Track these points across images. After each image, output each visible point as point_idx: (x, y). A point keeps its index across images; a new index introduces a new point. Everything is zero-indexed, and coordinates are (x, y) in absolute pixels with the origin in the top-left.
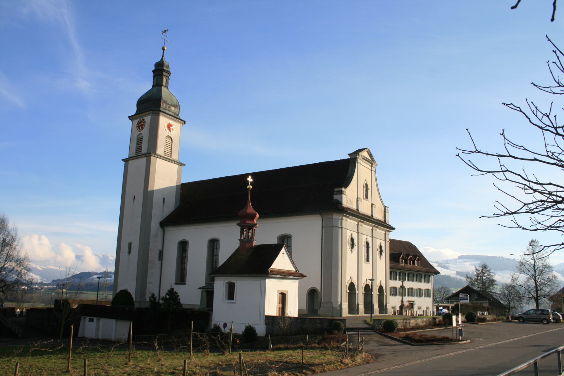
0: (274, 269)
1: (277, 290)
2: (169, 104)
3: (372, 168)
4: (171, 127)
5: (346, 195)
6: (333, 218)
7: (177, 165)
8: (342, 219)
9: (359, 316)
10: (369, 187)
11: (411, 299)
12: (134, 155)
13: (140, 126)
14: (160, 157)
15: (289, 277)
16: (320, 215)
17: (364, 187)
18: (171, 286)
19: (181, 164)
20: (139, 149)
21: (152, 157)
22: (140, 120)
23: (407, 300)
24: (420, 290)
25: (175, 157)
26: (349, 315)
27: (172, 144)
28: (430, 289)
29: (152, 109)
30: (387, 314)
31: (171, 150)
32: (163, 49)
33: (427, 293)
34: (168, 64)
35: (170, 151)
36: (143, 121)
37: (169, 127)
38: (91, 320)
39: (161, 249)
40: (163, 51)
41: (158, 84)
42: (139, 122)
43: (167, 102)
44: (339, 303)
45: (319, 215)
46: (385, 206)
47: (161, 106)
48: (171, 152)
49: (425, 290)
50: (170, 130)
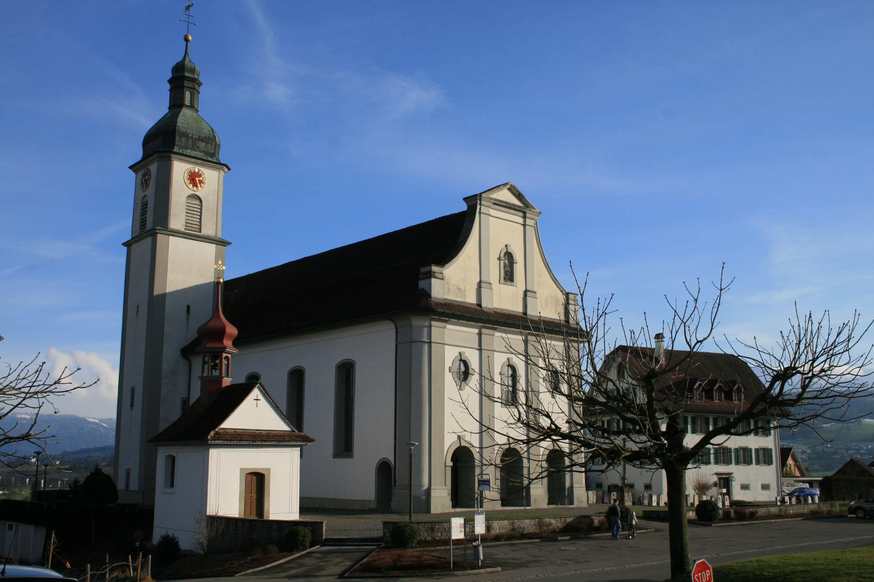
0: (229, 431)
1: (241, 469)
2: (192, 138)
3: (525, 221)
4: (197, 179)
6: (411, 326)
8: (430, 327)
9: (531, 509)
10: (519, 257)
11: (723, 469)
12: (137, 234)
13: (144, 183)
14: (176, 233)
15: (266, 443)
16: (390, 320)
17: (499, 259)
19: (221, 243)
20: (143, 222)
21: (158, 234)
22: (144, 171)
23: (714, 472)
24: (746, 451)
25: (208, 229)
27: (201, 209)
28: (770, 447)
29: (160, 150)
30: (573, 504)
31: (200, 219)
32: (187, 40)
33: (764, 457)
34: (193, 65)
36: (149, 170)
37: (193, 180)
38: (10, 527)
39: (185, 396)
41: (176, 105)
42: (144, 176)
43: (188, 134)
44: (426, 486)
46: (568, 292)
47: (177, 143)
48: (200, 222)
49: (757, 450)
50: (195, 185)
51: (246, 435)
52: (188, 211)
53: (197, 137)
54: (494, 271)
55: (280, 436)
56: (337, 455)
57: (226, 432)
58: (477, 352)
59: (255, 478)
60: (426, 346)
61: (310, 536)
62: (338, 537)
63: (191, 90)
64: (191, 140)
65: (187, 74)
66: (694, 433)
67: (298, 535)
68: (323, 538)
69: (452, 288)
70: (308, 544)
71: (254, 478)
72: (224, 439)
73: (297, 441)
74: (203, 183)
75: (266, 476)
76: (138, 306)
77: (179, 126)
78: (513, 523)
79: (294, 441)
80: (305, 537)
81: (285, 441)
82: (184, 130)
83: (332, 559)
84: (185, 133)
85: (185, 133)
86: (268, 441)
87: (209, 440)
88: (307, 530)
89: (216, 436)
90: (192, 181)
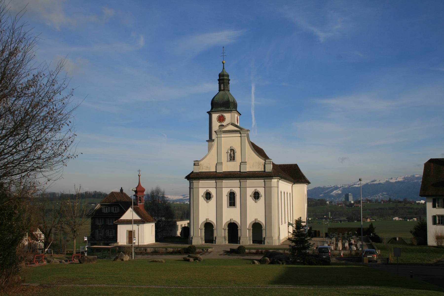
8: (193, 183)
54: (225, 157)
58: (215, 189)
66: (435, 225)
78: (155, 249)
79: (140, 222)
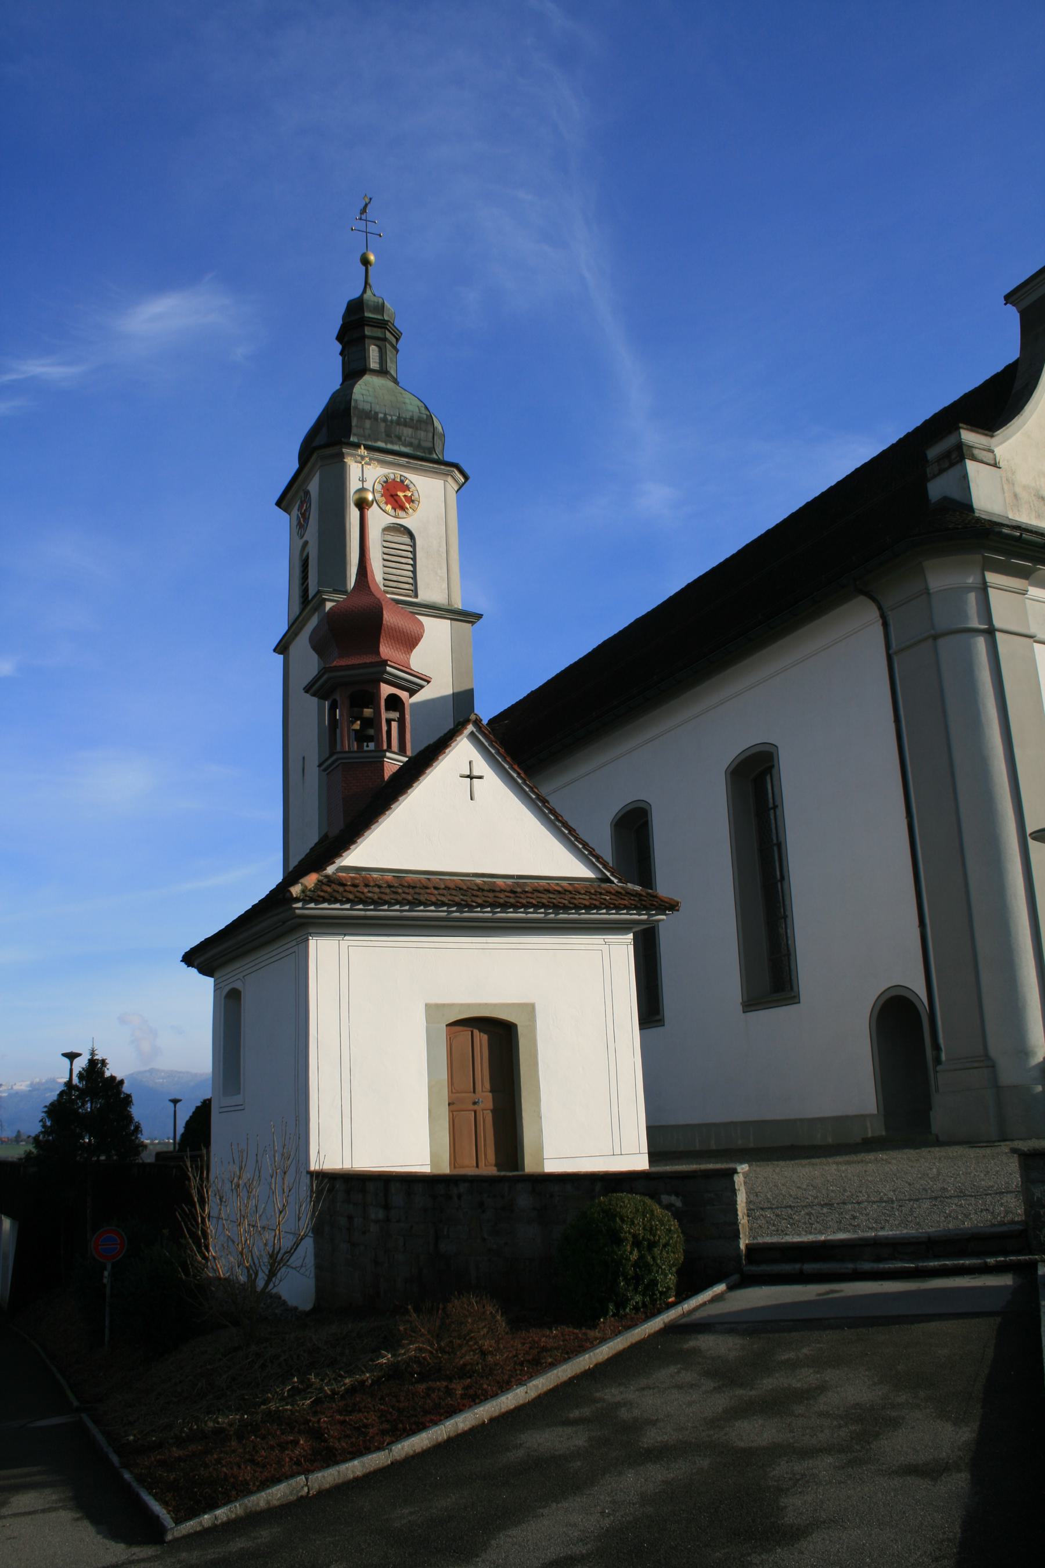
0: (375, 875)
1: (428, 1006)
2: (385, 420)
4: (401, 494)
5: (995, 465)
6: (927, 592)
7: (447, 623)
18: (93, 1054)
26: (731, 1165)
27: (414, 553)
31: (414, 572)
32: (365, 262)
34: (380, 300)
35: (410, 574)
37: (392, 496)
40: (364, 268)
43: (376, 413)
45: (862, 598)
47: (354, 430)
48: (415, 578)
50: (399, 506)
51: (436, 888)
52: (386, 557)
53: (395, 418)
55: (559, 892)
56: (751, 1003)
57: (364, 878)
59: (485, 1037)
60: (981, 644)
61: (677, 1237)
62: (811, 1238)
63: (379, 343)
64: (383, 425)
65: (368, 314)
67: (616, 1239)
68: (742, 1246)
69: (1024, 495)
70: (672, 1278)
71: (482, 1039)
72: (351, 896)
73: (618, 908)
74: (413, 501)
75: (520, 1030)
76: (304, 758)
77: (356, 401)
80: (652, 1245)
81: (577, 908)
82: (367, 407)
83: (806, 1378)
84: (371, 411)
85: (371, 411)
86: (515, 907)
87: (297, 900)
88: (658, 1210)
89: (326, 888)
90: (392, 499)
